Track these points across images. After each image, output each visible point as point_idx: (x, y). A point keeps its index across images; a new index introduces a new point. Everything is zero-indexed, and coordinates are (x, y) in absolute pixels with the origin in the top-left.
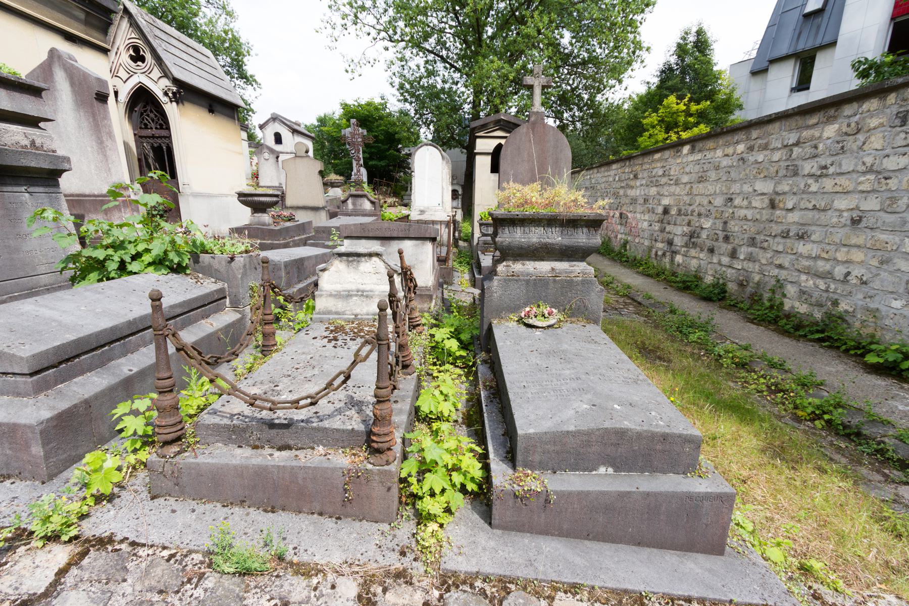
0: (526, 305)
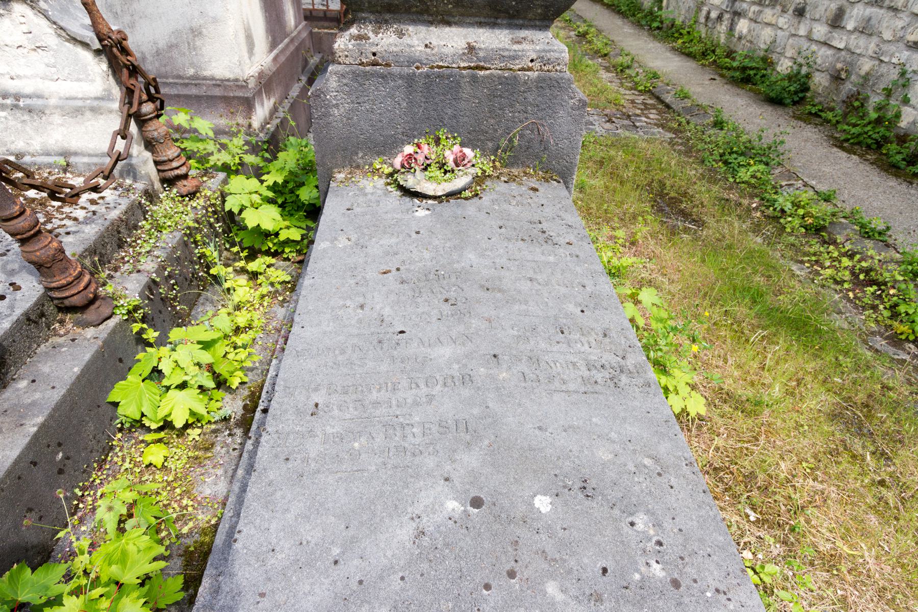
0: (409, 137)
